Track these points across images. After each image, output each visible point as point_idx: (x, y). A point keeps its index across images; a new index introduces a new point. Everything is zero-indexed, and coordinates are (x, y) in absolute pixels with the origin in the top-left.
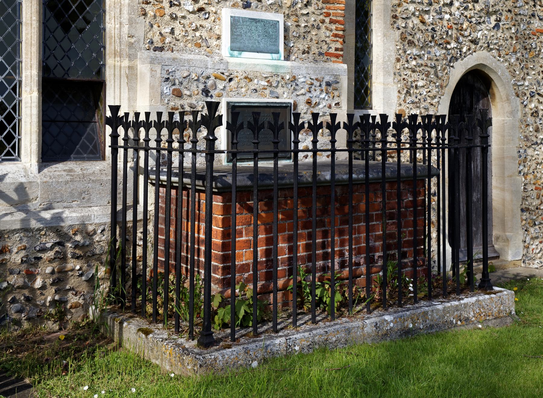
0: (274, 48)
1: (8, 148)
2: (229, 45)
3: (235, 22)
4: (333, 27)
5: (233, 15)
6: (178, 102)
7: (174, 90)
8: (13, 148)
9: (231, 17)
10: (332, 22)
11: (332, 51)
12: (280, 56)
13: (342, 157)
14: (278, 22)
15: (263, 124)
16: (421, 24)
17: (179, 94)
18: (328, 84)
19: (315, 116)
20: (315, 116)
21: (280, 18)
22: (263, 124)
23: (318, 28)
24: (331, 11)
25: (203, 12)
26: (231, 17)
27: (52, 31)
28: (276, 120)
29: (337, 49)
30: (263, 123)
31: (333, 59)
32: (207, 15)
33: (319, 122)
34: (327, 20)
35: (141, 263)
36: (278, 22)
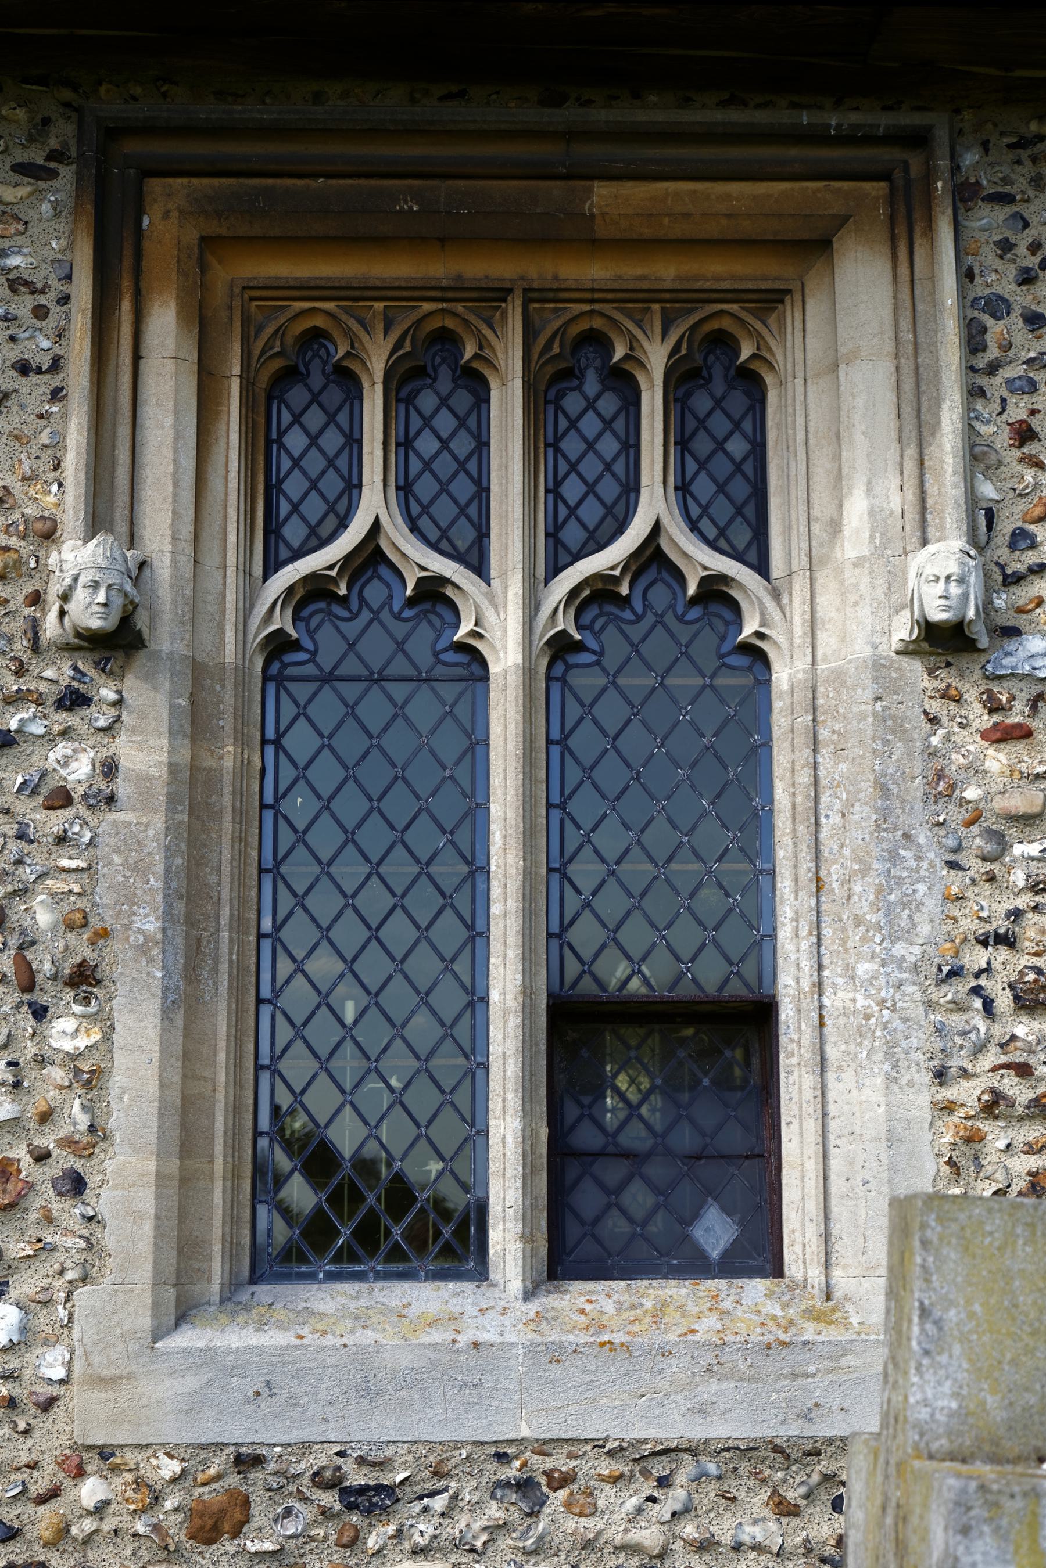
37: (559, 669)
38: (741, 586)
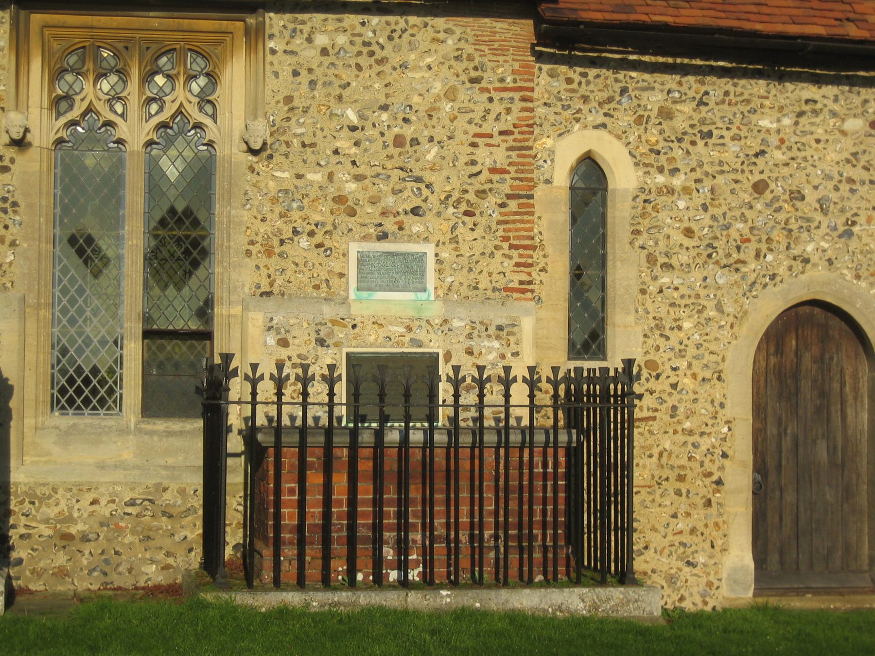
0: (419, 286)
1: (110, 402)
2: (356, 285)
3: (362, 260)
4: (515, 253)
5: (360, 250)
6: (284, 353)
7: (279, 340)
8: (115, 402)
9: (358, 252)
10: (511, 247)
11: (515, 285)
12: (429, 296)
13: (545, 419)
14: (426, 253)
15: (515, 378)
16: (754, 253)
17: (284, 343)
18: (500, 328)
19: (481, 369)
20: (481, 369)
21: (429, 250)
22: (515, 378)
23: (492, 255)
24: (511, 234)
25: (323, 249)
26: (358, 252)
27: (202, 287)
28: (481, 375)
29: (521, 283)
30: (516, 377)
31: (516, 295)
32: (329, 252)
33: (485, 376)
34: (505, 245)
35: (392, 510)
36: (426, 253)
37: (149, 148)
38: (206, 126)
